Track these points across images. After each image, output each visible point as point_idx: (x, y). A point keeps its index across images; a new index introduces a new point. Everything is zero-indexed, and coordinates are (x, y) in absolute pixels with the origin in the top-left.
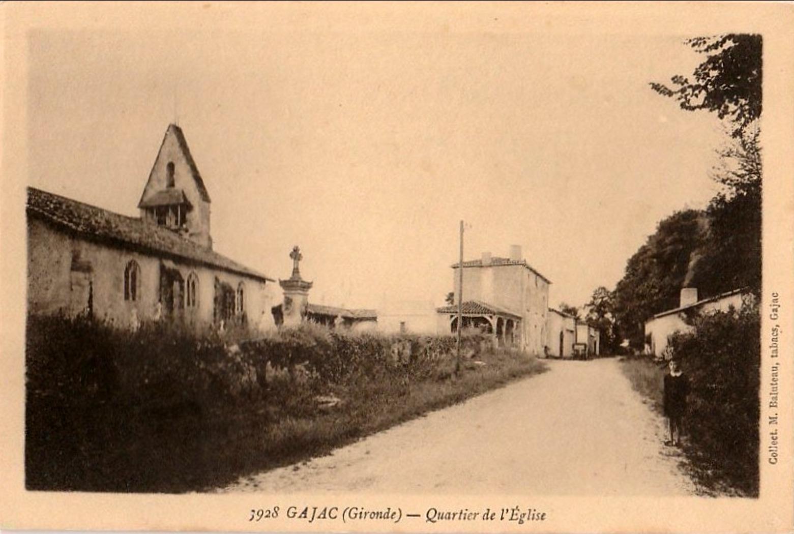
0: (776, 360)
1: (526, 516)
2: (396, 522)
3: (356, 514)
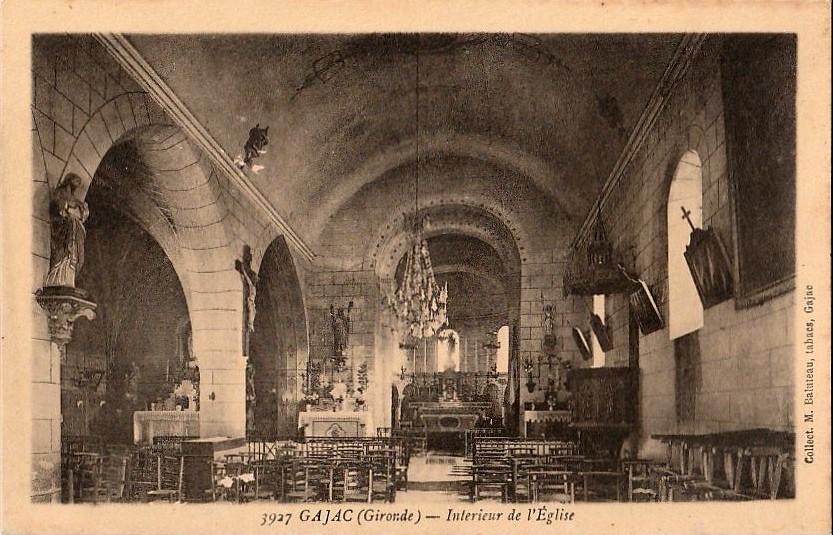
0: (810, 356)
1: (554, 516)
2: (416, 523)
3: (308, 517)
